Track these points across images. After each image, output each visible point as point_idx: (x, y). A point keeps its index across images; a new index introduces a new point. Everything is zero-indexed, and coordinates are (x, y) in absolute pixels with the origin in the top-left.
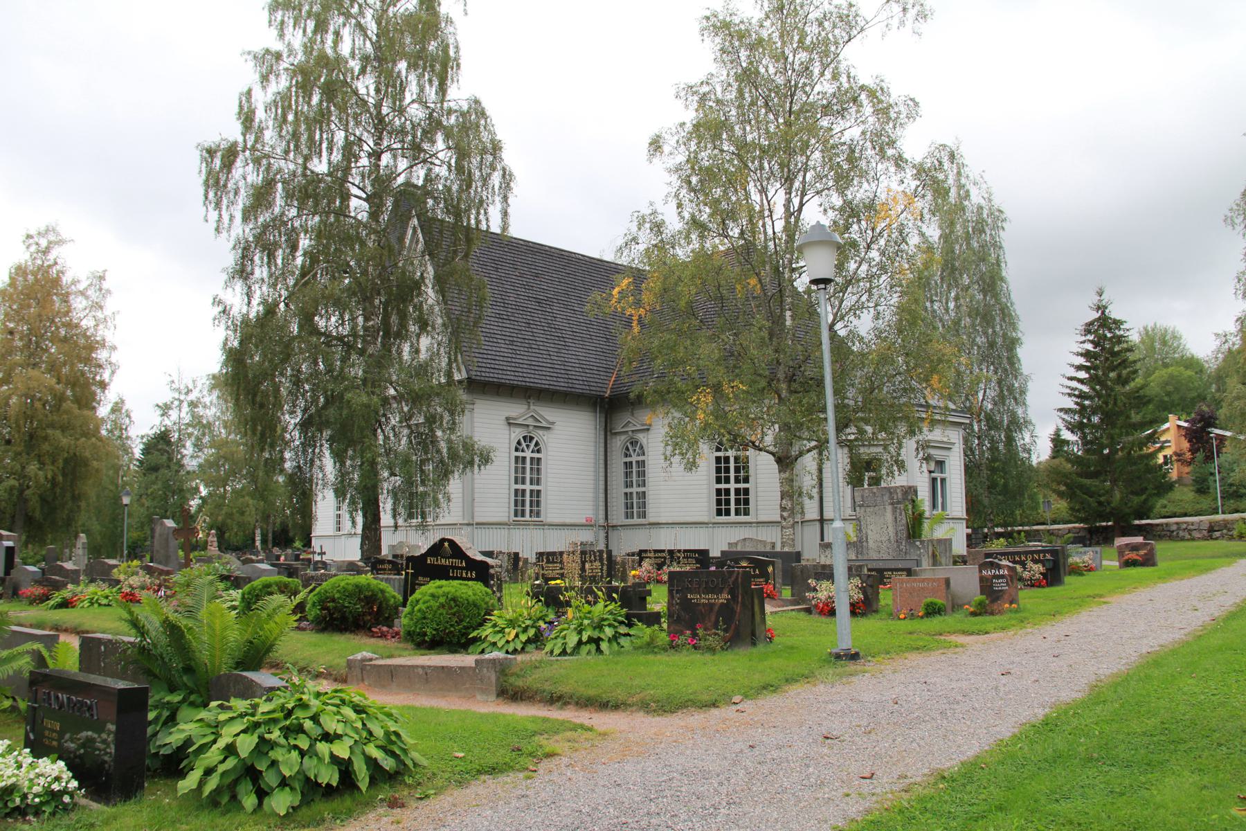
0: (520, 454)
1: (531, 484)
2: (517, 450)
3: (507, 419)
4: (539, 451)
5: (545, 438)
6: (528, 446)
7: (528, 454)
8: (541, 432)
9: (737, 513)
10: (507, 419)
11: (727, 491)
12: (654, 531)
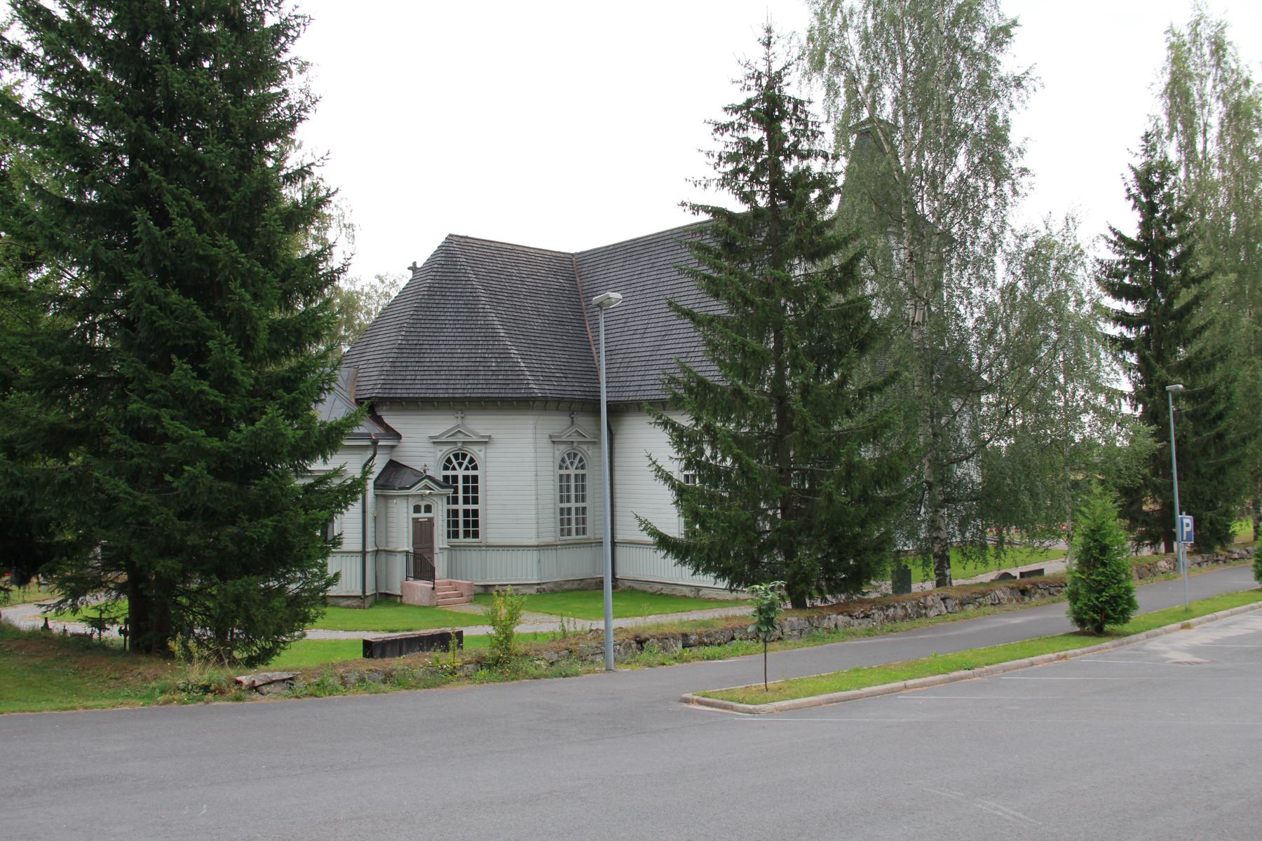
1: (576, 501)
2: (561, 467)
3: (551, 437)
4: (583, 467)
6: (572, 463)
8: (475, 448)
9: (467, 534)
12: (492, 556)
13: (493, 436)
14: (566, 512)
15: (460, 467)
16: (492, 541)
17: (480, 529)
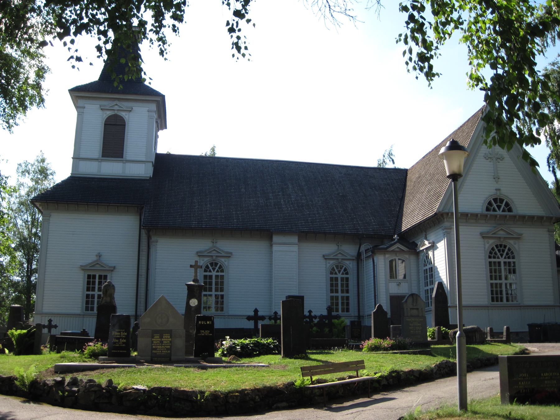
0: (334, 276)
2: (331, 273)
5: (516, 246)
7: (339, 276)
8: (223, 260)
10: (324, 256)
13: (233, 254)
14: (498, 286)
15: (339, 273)
16: (231, 313)
17: (224, 306)
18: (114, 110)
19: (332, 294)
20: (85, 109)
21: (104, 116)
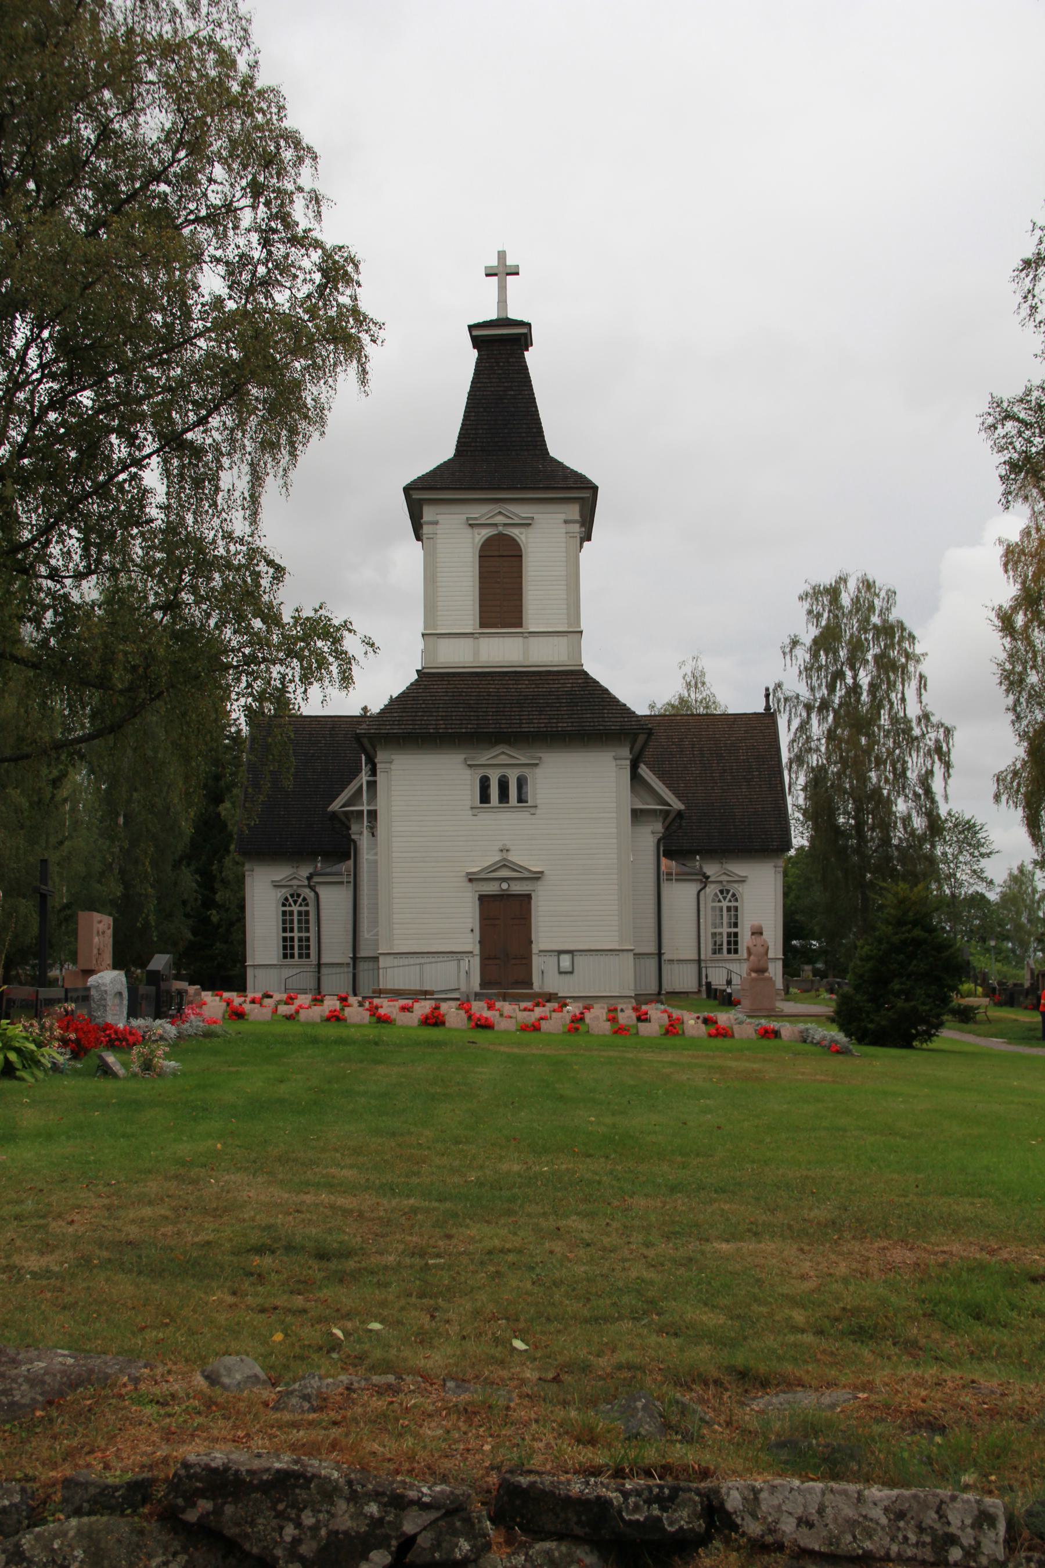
0: (287, 909)
2: (284, 905)
7: (295, 909)
8: (736, 885)
9: (729, 952)
11: (292, 939)
18: (495, 525)
19: (285, 935)
20: (438, 527)
21: (477, 540)
